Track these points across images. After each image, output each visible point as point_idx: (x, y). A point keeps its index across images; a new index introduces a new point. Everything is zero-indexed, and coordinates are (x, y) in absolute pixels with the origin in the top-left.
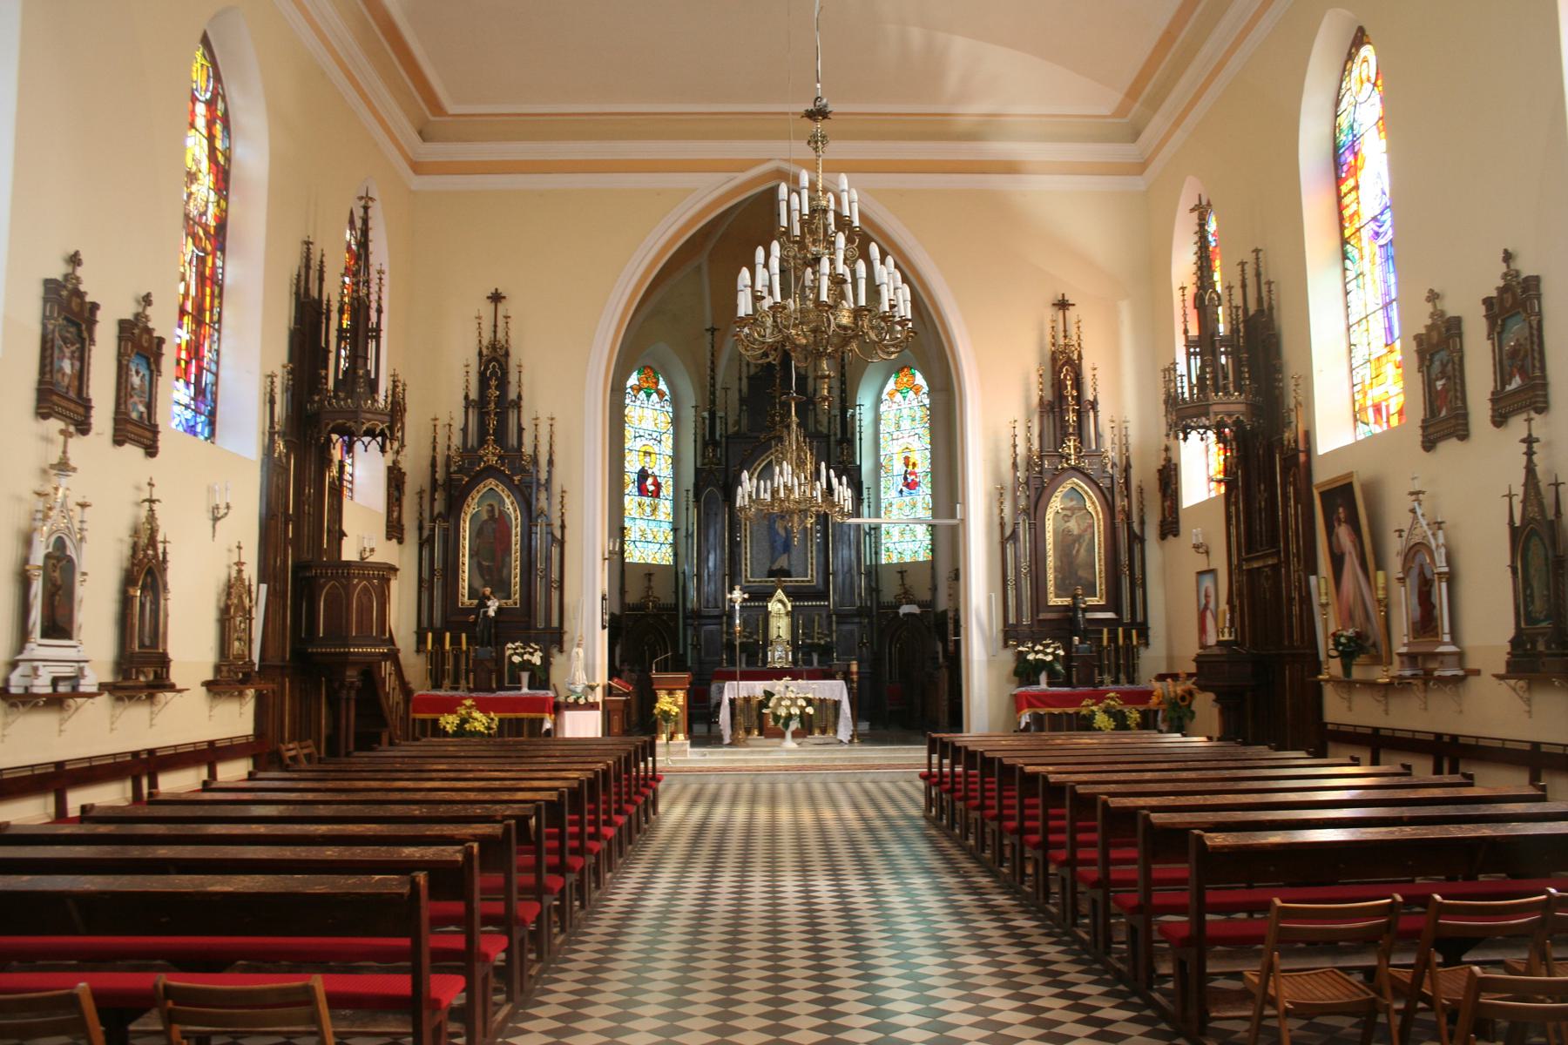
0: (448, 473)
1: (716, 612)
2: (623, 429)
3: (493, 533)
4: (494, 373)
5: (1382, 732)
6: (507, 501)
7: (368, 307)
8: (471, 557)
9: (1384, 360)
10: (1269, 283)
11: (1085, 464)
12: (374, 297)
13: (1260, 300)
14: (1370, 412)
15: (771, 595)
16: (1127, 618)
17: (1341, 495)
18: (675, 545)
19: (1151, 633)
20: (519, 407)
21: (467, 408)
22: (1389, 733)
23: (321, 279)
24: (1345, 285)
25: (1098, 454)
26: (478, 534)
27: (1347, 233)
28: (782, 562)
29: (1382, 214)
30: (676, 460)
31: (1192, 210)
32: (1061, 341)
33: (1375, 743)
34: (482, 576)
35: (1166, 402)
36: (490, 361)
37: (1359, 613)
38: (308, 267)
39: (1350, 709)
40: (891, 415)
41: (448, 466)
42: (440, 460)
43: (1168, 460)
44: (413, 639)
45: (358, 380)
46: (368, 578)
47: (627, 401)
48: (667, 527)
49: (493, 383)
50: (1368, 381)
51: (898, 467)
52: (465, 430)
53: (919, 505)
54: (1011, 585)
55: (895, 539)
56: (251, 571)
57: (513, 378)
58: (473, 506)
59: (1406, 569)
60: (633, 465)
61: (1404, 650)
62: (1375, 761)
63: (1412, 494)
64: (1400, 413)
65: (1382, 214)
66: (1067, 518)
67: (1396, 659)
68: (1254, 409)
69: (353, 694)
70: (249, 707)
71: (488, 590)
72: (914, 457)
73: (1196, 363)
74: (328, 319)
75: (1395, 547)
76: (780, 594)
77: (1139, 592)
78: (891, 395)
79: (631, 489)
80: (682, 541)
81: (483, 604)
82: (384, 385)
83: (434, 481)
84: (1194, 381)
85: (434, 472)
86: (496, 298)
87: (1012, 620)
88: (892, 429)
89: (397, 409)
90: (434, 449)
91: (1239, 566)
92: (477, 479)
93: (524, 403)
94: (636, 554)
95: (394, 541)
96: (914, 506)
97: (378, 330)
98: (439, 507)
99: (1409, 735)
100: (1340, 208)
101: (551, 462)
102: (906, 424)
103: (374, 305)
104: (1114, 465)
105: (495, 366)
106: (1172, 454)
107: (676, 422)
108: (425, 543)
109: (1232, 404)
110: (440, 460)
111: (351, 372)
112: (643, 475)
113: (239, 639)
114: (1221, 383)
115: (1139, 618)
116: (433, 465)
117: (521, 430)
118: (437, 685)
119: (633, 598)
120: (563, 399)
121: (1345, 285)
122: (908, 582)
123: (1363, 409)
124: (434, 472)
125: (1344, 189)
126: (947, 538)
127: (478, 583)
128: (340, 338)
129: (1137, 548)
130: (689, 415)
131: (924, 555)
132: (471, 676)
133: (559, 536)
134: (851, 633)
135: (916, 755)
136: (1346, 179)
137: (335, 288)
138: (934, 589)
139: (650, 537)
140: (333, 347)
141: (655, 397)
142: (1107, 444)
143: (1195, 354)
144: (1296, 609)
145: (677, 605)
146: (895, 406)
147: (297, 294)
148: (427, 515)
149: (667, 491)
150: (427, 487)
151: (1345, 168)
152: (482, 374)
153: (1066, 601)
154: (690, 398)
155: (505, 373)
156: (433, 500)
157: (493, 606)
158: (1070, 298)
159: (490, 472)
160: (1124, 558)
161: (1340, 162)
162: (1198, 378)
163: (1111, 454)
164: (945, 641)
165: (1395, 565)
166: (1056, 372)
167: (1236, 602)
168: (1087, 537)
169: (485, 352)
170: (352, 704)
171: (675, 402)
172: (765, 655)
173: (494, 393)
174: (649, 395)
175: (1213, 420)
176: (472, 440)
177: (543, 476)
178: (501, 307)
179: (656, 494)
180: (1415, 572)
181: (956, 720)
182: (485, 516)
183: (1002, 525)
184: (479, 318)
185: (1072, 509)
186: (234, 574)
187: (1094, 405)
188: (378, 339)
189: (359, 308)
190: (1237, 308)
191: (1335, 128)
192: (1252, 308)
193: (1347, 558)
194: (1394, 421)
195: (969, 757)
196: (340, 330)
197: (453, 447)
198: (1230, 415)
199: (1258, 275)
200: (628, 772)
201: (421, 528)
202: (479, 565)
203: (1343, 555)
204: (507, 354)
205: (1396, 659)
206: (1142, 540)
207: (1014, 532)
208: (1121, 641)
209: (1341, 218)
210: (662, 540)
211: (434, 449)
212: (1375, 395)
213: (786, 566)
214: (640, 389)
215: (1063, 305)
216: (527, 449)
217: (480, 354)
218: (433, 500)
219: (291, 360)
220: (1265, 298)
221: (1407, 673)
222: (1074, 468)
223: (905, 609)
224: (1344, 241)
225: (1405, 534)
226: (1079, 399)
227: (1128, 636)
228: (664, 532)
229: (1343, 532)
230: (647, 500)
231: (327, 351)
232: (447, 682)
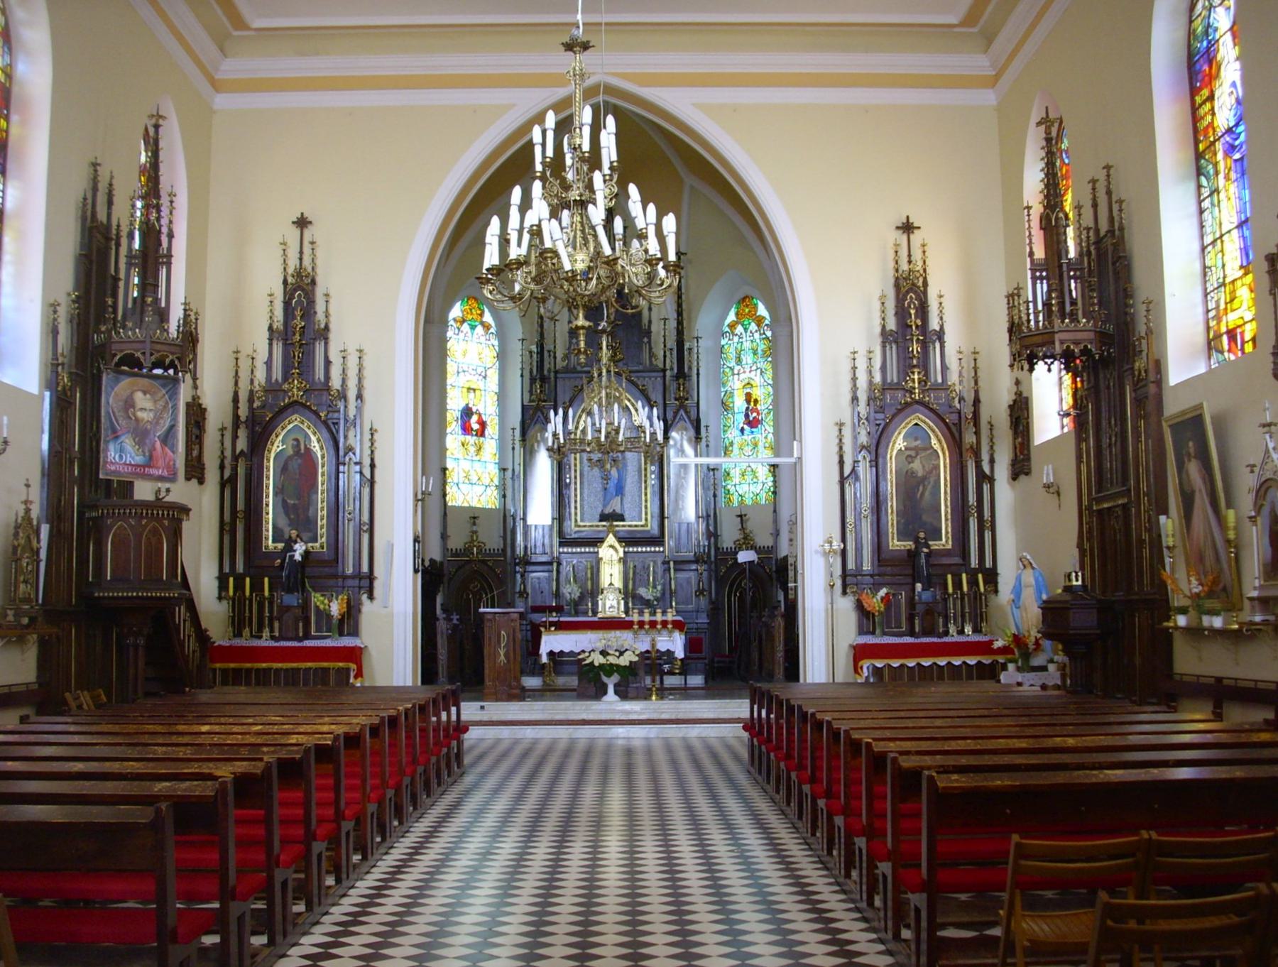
0: (251, 409)
1: (544, 559)
2: (445, 364)
3: (300, 468)
4: (299, 302)
5: (1225, 682)
6: (313, 438)
7: (160, 232)
8: (275, 494)
9: (1239, 283)
10: (1120, 202)
11: (930, 398)
12: (164, 222)
13: (1111, 219)
14: (1225, 339)
15: (602, 541)
16: (974, 562)
17: (1192, 424)
18: (502, 488)
19: (1000, 579)
20: (326, 339)
21: (271, 340)
22: (1232, 683)
23: (110, 203)
24: (1200, 202)
25: (944, 387)
26: (283, 469)
27: (1201, 147)
28: (615, 505)
29: (1237, 125)
30: (502, 396)
31: (1039, 124)
32: (904, 266)
33: (1221, 694)
34: (287, 514)
35: (1010, 331)
36: (295, 290)
37: (1209, 554)
38: (95, 189)
39: (1200, 659)
40: (732, 350)
41: (251, 400)
42: (243, 396)
43: (1019, 394)
44: (215, 584)
45: (151, 305)
46: (159, 519)
47: (450, 334)
48: (494, 470)
49: (298, 313)
50: (1222, 306)
51: (739, 403)
52: (269, 363)
53: (761, 445)
54: (849, 528)
55: (737, 480)
56: (35, 512)
57: (320, 307)
58: (277, 445)
59: (1258, 508)
60: (455, 403)
61: (1255, 594)
62: (1218, 717)
63: (1264, 426)
64: (1254, 340)
65: (1237, 125)
66: (910, 459)
67: (1247, 604)
68: (1103, 338)
69: (141, 641)
70: (31, 654)
71: (294, 533)
72: (757, 393)
73: (1042, 288)
74: (118, 245)
75: (1246, 483)
76: (611, 539)
77: (988, 535)
78: (732, 326)
79: (453, 427)
80: (509, 482)
81: (289, 548)
82: (176, 314)
83: (236, 417)
84: (1040, 307)
85: (236, 408)
86: (302, 223)
87: (851, 565)
88: (732, 364)
89: (190, 338)
90: (236, 383)
91: (1089, 508)
92: (282, 413)
93: (332, 336)
94: (459, 496)
95: (194, 481)
96: (756, 445)
97: (169, 256)
98: (242, 444)
99: (1252, 685)
100: (1195, 119)
101: (359, 397)
102: (748, 358)
103: (165, 230)
104: (961, 399)
105: (300, 292)
106: (1023, 388)
107: (502, 356)
108: (227, 483)
109: (1080, 331)
110: (243, 396)
111: (140, 302)
112: (467, 412)
113: (26, 582)
114: (1068, 308)
115: (988, 564)
116: (236, 400)
117: (328, 363)
118: (238, 634)
119: (456, 542)
120: (372, 330)
121: (1200, 202)
122: (750, 526)
123: (1218, 336)
124: (236, 408)
125: (1198, 99)
126: (784, 477)
127: (283, 522)
128: (129, 265)
129: (986, 488)
130: (516, 349)
131: (764, 498)
132: (276, 625)
133: (368, 475)
134: (688, 581)
135: (741, 708)
136: (1200, 89)
137: (128, 212)
138: (777, 534)
139: (474, 479)
140: (122, 275)
141: (480, 329)
142: (953, 378)
143: (1041, 278)
144: (1146, 552)
145: (504, 550)
146: (736, 339)
147: (84, 219)
148: (228, 453)
149: (492, 430)
150: (229, 423)
151: (1200, 77)
152: (287, 304)
153: (909, 545)
154: (517, 330)
155: (311, 302)
156: (235, 437)
157: (299, 549)
158: (915, 221)
159: (294, 406)
160: (972, 499)
161: (1198, 68)
162: (1044, 305)
163: (957, 388)
164: (786, 589)
165: (1246, 502)
166: (900, 300)
167: (1087, 546)
168: (932, 480)
169: (290, 280)
170: (141, 652)
171: (502, 335)
172: (595, 604)
173: (299, 323)
174: (473, 328)
175: (1058, 349)
176: (277, 374)
177: (352, 412)
178: (307, 233)
179: (481, 433)
180: (1266, 510)
181: (792, 670)
182: (290, 452)
183: (841, 463)
184: (284, 244)
185: (917, 450)
186: (21, 513)
187: (940, 335)
188: (169, 264)
189: (151, 234)
190: (1088, 229)
191: (1191, 34)
192: (1104, 226)
193: (1197, 496)
194: (1249, 348)
195: (794, 714)
196: (130, 256)
197: (256, 383)
198: (1076, 343)
199: (1109, 193)
200: (425, 718)
201: (222, 467)
202: (284, 502)
203: (1193, 492)
204: (313, 282)
205: (1247, 604)
206: (991, 480)
207: (853, 470)
208: (965, 588)
209: (1196, 131)
210: (487, 482)
211: (236, 383)
212: (1232, 319)
213: (618, 511)
214: (463, 321)
215: (908, 228)
216: (336, 383)
217: (285, 282)
218: (235, 437)
219: (76, 288)
220: (1116, 218)
221: (1258, 619)
222: (918, 402)
223: (744, 556)
224: (1199, 156)
225: (1256, 470)
226: (924, 327)
227: (973, 583)
228: (491, 472)
229: (1193, 468)
230: (471, 439)
231: (116, 279)
232: (246, 632)
